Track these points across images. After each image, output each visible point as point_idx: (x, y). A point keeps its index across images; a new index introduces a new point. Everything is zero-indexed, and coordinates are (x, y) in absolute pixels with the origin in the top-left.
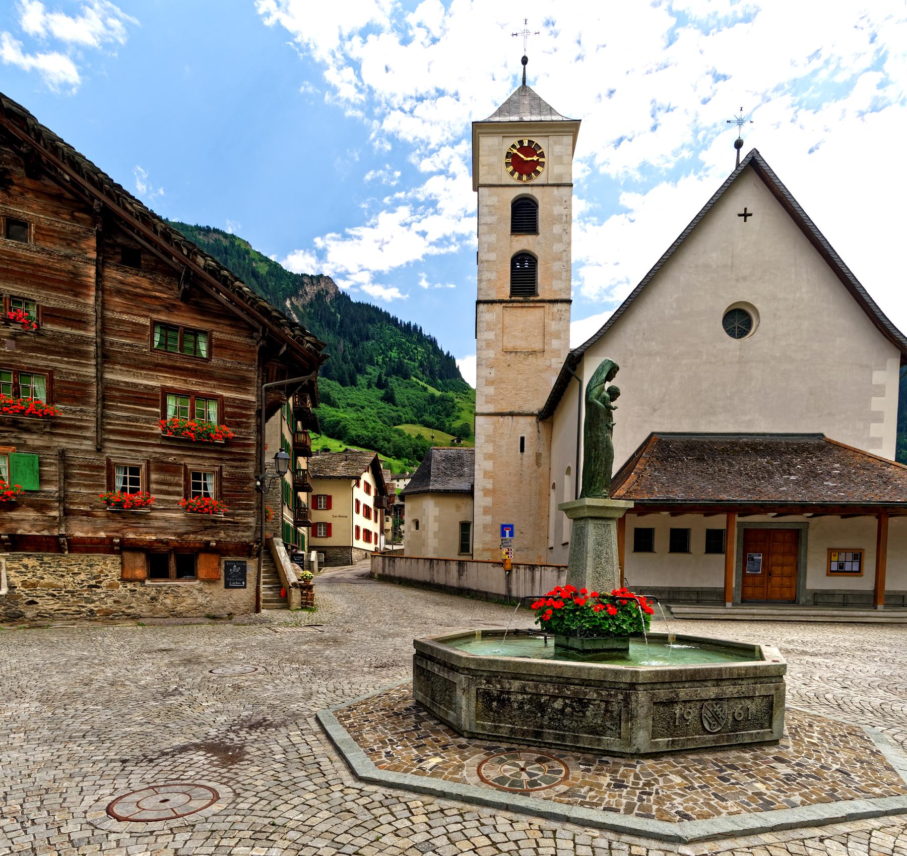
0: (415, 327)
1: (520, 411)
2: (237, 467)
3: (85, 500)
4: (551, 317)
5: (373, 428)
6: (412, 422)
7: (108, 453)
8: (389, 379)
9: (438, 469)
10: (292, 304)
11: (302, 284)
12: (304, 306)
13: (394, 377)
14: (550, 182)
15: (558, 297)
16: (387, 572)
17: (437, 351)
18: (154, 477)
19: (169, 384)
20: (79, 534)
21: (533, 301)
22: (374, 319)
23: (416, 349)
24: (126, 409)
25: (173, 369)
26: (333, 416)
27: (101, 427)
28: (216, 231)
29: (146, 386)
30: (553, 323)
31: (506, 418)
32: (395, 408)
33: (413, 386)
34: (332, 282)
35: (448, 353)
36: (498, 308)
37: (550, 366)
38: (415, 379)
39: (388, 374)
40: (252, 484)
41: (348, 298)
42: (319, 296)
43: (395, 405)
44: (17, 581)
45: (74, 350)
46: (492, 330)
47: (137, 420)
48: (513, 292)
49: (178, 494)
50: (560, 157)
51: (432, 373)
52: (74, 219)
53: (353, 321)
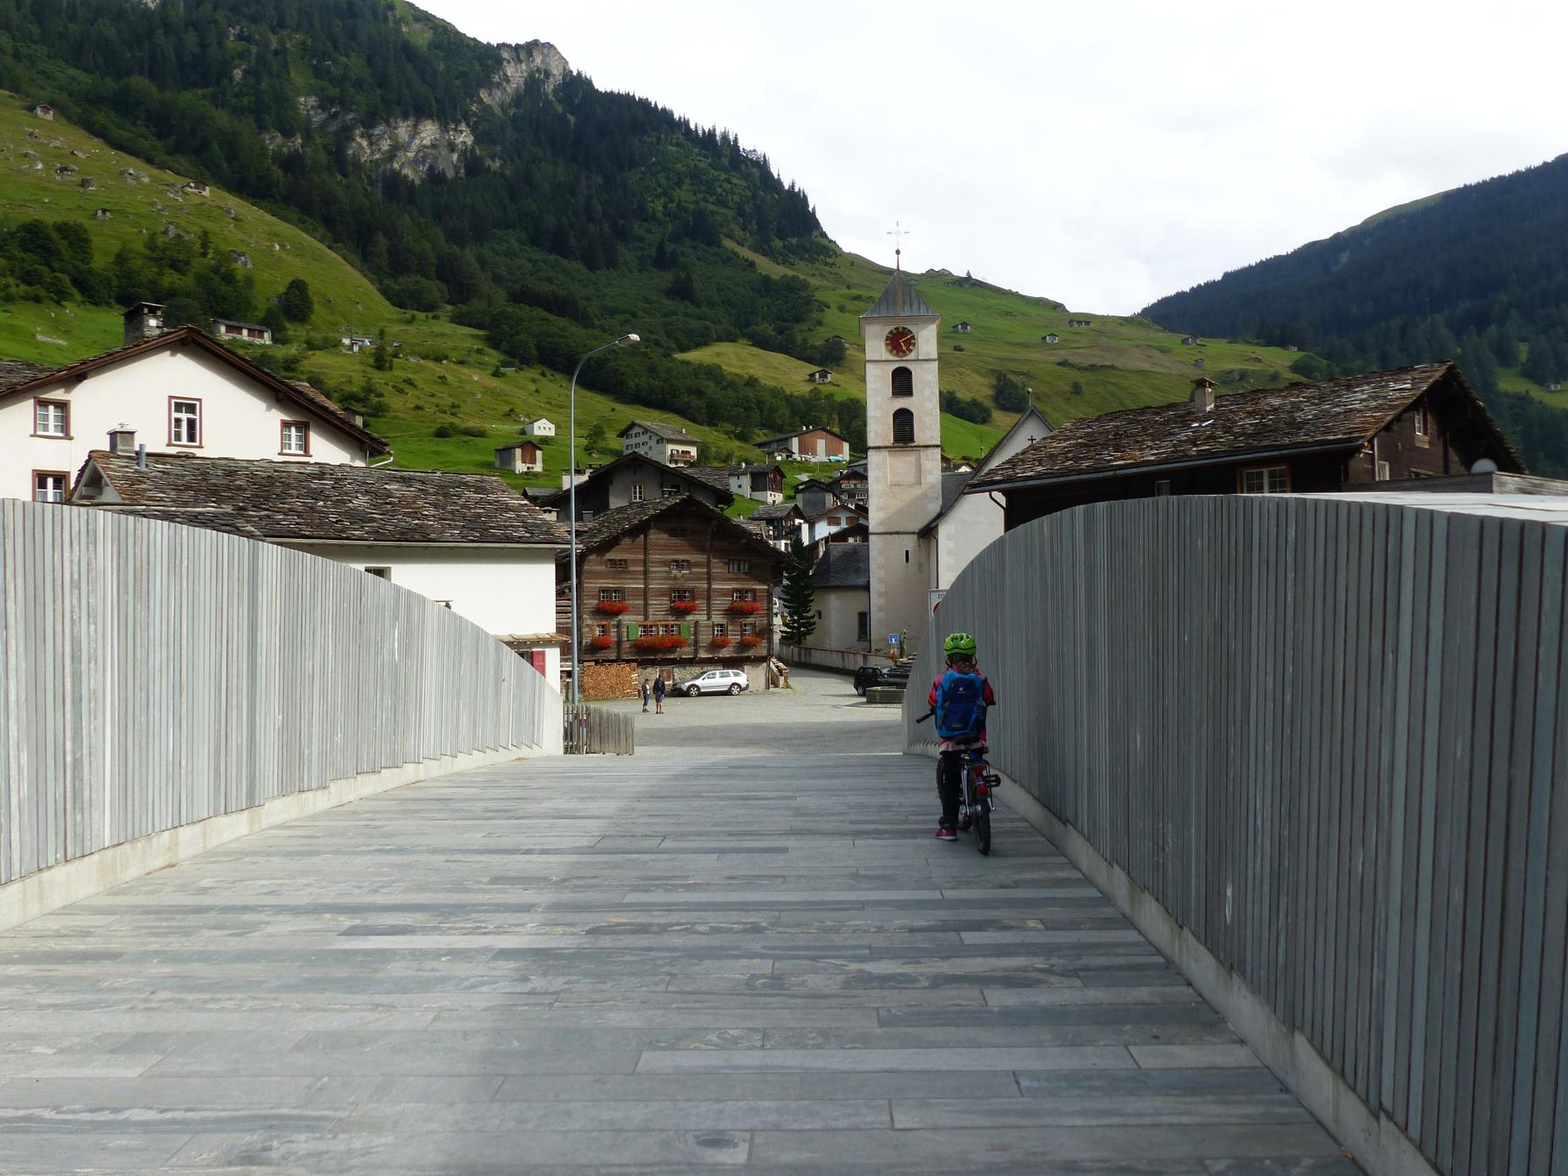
0: (725, 137)
7: (713, 619)
13: (688, 241)
16: (803, 659)
17: (772, 184)
23: (729, 181)
33: (727, 261)
36: (885, 453)
42: (533, 84)
48: (896, 439)
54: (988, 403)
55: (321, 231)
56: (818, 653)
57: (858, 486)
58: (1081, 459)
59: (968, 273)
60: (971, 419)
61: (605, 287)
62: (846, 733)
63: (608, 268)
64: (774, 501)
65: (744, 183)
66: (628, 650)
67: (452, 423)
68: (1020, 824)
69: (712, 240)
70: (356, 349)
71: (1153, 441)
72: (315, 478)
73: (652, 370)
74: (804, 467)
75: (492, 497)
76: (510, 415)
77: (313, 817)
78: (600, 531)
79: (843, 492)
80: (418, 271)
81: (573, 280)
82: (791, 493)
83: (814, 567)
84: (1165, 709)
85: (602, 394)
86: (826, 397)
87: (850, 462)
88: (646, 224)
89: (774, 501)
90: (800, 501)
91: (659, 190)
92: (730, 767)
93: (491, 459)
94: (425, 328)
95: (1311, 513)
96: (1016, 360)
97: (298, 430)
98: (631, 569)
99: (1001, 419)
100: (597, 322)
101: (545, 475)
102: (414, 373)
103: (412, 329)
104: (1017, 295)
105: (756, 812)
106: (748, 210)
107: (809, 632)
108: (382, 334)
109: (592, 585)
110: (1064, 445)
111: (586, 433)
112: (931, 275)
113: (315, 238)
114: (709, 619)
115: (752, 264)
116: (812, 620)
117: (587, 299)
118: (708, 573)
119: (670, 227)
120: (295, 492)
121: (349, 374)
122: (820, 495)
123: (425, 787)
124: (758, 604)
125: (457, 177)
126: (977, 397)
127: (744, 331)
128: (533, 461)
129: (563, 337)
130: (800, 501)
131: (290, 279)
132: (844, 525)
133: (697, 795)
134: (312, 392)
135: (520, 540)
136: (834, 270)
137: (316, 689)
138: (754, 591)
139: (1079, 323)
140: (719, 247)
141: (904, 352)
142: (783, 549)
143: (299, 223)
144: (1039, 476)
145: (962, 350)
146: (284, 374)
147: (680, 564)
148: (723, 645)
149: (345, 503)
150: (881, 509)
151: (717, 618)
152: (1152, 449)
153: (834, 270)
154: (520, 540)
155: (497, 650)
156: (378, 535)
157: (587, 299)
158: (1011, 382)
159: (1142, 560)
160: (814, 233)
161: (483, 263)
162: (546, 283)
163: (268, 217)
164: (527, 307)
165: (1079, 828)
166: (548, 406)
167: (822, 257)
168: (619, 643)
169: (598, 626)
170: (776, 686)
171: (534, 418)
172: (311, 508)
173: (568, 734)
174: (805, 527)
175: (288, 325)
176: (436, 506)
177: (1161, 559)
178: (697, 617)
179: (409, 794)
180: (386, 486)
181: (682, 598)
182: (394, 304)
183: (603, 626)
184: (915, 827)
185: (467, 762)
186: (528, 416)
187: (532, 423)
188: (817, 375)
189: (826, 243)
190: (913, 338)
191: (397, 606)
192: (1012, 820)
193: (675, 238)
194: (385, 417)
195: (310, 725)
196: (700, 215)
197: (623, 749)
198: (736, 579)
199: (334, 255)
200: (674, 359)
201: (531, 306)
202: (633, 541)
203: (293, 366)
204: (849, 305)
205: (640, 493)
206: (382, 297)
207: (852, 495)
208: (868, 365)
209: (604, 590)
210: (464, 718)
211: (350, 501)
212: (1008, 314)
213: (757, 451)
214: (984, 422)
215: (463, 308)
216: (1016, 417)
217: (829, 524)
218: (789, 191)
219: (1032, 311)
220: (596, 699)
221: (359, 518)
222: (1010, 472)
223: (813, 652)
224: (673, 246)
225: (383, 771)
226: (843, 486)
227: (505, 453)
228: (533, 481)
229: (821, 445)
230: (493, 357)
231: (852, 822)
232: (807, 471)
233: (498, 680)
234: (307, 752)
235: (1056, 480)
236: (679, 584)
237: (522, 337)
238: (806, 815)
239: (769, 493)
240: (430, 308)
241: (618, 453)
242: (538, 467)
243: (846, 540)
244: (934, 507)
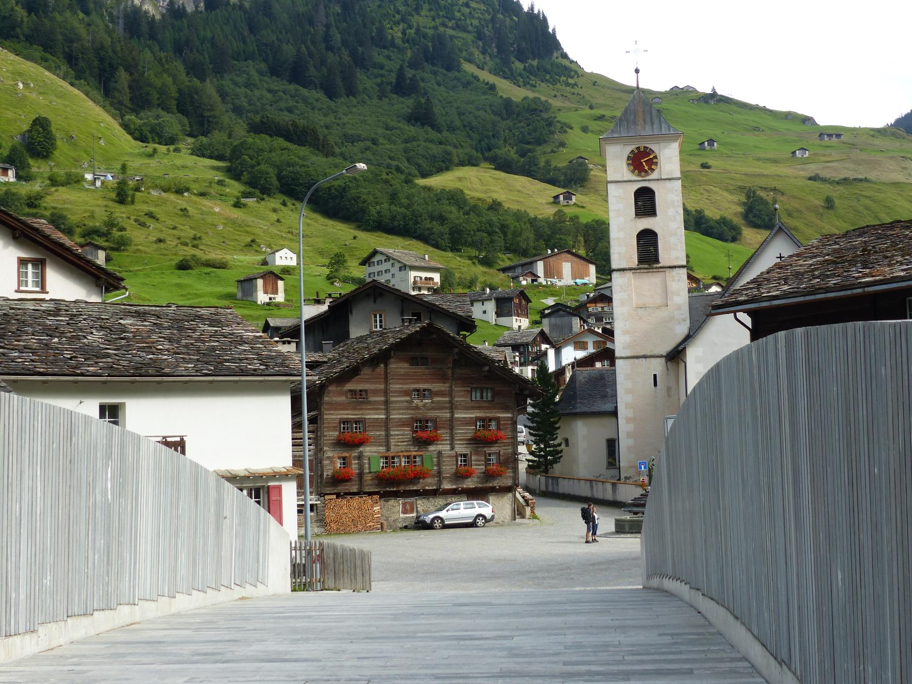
1: (652, 354)
2: (506, 449)
8: (419, 74)
13: (428, 67)
16: (550, 489)
21: (656, 268)
24: (462, 429)
30: (674, 283)
36: (629, 274)
43: (436, 128)
48: (641, 261)
51: (501, 50)
54: (738, 221)
55: (64, 68)
56: (566, 482)
57: (606, 309)
58: (828, 276)
59: (714, 89)
60: (721, 238)
61: (346, 115)
62: (593, 565)
63: (348, 96)
64: (520, 327)
65: (483, 7)
66: (370, 482)
67: (194, 256)
68: (741, 664)
69: (451, 65)
70: (98, 183)
71: (903, 256)
72: (50, 315)
73: (393, 197)
74: (550, 291)
75: (227, 330)
76: (252, 245)
77: (19, 663)
78: (339, 362)
79: (589, 315)
80: (159, 105)
81: (313, 109)
82: (537, 318)
83: (561, 393)
84: (861, 543)
85: (343, 223)
86: (571, 219)
87: (597, 285)
88: (386, 52)
89: (520, 327)
90: (546, 326)
91: (398, 17)
92: (455, 605)
93: (233, 289)
94: (166, 161)
95: (295, 442)
96: (767, 176)
97: (35, 266)
98: (372, 399)
99: (752, 236)
100: (337, 150)
101: (288, 306)
102: (156, 206)
103: (152, 162)
104: (764, 110)
105: (467, 653)
106: (487, 33)
107: (556, 461)
108: (124, 168)
109: (332, 416)
110: (810, 262)
111: (327, 261)
112: (677, 94)
113: (58, 76)
114: (452, 448)
115: (492, 88)
116: (559, 448)
117: (327, 127)
118: (451, 402)
119: (409, 53)
120: (30, 330)
121: (92, 208)
122: (566, 319)
123: (138, 630)
124: (502, 433)
125: (197, 11)
126: (726, 215)
127: (486, 154)
128: (275, 292)
129: (303, 166)
130: (546, 326)
131: (34, 117)
132: (591, 350)
133: (411, 636)
134: (49, 230)
135: (255, 373)
136: (576, 90)
137: (24, 531)
138: (498, 420)
139: (830, 136)
140: (459, 71)
141: (646, 171)
142: (530, 375)
143: (43, 62)
144: (785, 296)
145: (708, 167)
146: (27, 210)
147: (421, 394)
148: (466, 476)
149: (79, 339)
150: (627, 332)
151: (460, 449)
152: (902, 264)
153: (576, 90)
154: (255, 373)
155: (218, 488)
156: (112, 371)
157: (327, 127)
158: (761, 198)
159: (835, 389)
160: (555, 55)
161: (223, 95)
162: (286, 113)
163: (12, 56)
164: (267, 137)
165: (793, 668)
166: (290, 235)
167: (563, 78)
168: (361, 475)
169: (339, 458)
170: (523, 517)
171: (276, 248)
172: (46, 345)
173: (297, 570)
174: (551, 353)
175: (31, 162)
176: (170, 340)
177: (851, 387)
178: (440, 447)
179: (121, 637)
180: (122, 321)
181: (424, 428)
182: (136, 139)
183: (344, 458)
184: (629, 668)
185: (183, 603)
186: (269, 246)
187: (274, 253)
188: (561, 197)
189: (565, 62)
190: (656, 157)
191: (110, 446)
192: (732, 660)
193: (413, 65)
194: (127, 250)
195: (18, 568)
196: (440, 41)
197: (360, 585)
198: (479, 408)
199: (76, 91)
200: (416, 185)
201: (271, 136)
202: (373, 371)
203: (36, 203)
204: (593, 125)
205: (381, 321)
206: (124, 132)
207: (599, 319)
208: (610, 186)
209: (345, 422)
210: (183, 557)
211: (85, 337)
212: (756, 129)
213: (502, 275)
214: (734, 240)
215: (204, 139)
216: (765, 233)
217: (576, 349)
218: (528, 13)
219: (781, 125)
220: (338, 533)
221: (94, 354)
222: (755, 292)
223: (560, 481)
224: (413, 72)
225: (96, 613)
226: (590, 310)
227: (247, 284)
228: (276, 312)
229: (567, 268)
230: (235, 188)
231: (565, 664)
232: (553, 295)
233: (220, 517)
234: (13, 595)
235: (802, 299)
236: (419, 414)
237: (263, 167)
238: (517, 656)
239: (514, 318)
240: (171, 141)
241: (360, 281)
242: (280, 298)
243: (593, 365)
244: (682, 329)
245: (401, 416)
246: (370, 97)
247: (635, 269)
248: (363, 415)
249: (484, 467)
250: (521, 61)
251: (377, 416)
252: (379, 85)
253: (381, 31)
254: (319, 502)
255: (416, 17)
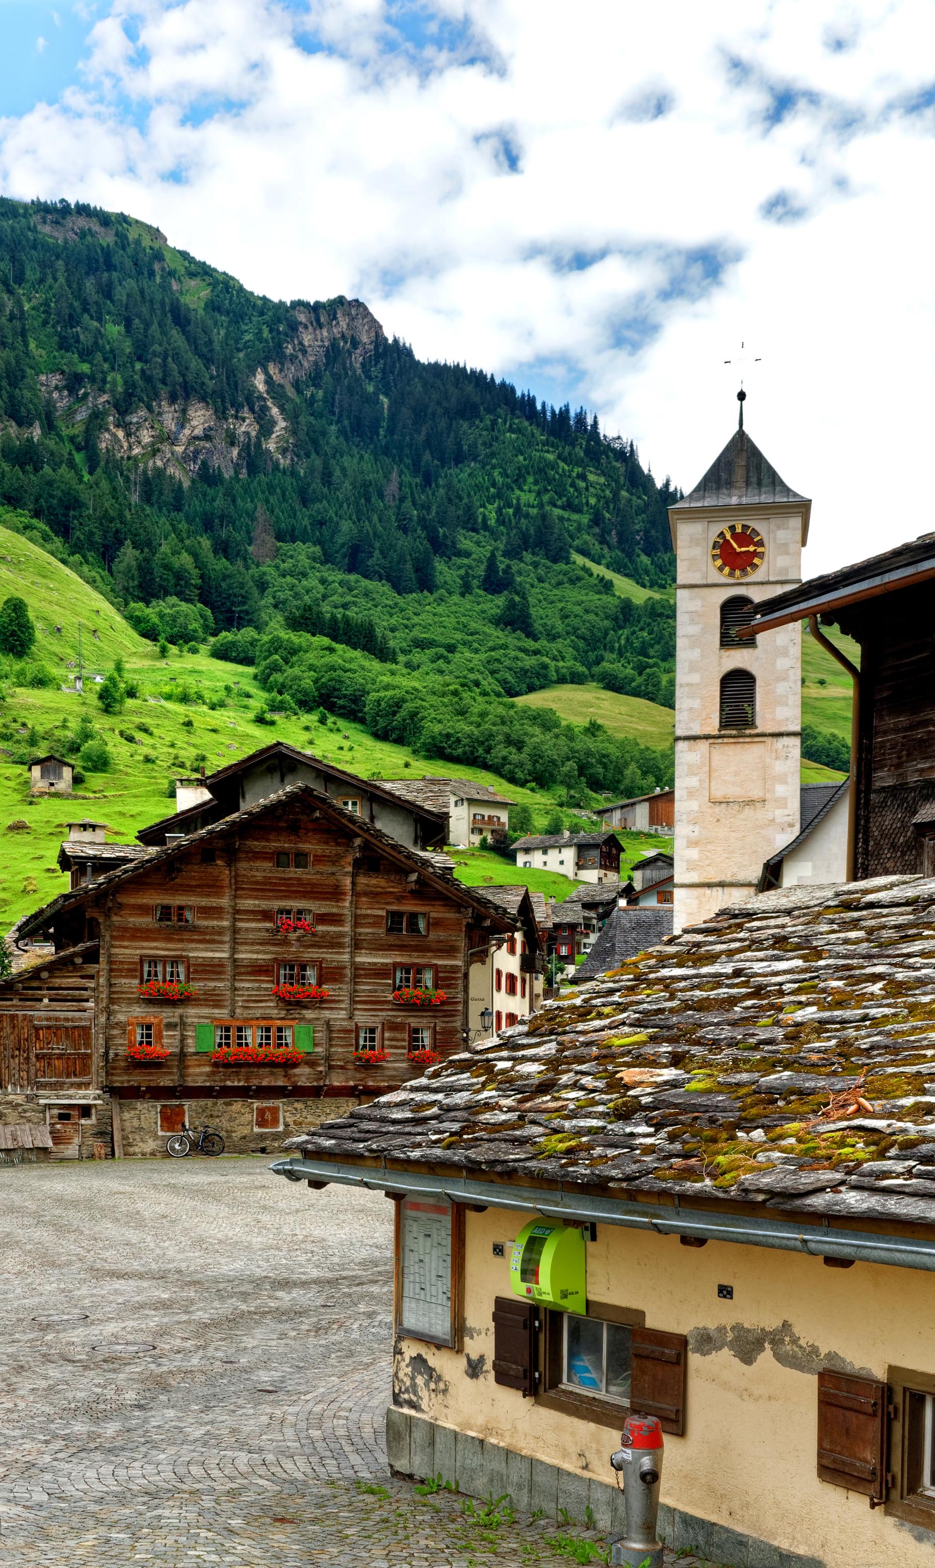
3: (341, 1056)
4: (774, 755)
5: (483, 715)
6: (576, 679)
8: (516, 566)
9: (626, 942)
10: (269, 381)
11: (294, 327)
12: (297, 385)
14: (772, 579)
15: (783, 729)
18: (387, 1035)
19: (398, 960)
20: (336, 1084)
21: (750, 736)
22: (475, 407)
23: (583, 477)
24: (368, 983)
25: (402, 948)
26: (387, 687)
27: (353, 1002)
28: (83, 210)
29: (382, 964)
30: (778, 762)
31: (715, 889)
32: (530, 644)
34: (367, 313)
35: (667, 485)
36: (703, 745)
37: (773, 820)
38: (580, 560)
39: (512, 553)
40: (459, 1036)
41: (409, 353)
42: (333, 353)
43: (531, 635)
44: (290, 1120)
45: (334, 943)
46: (696, 774)
47: (376, 991)
48: (724, 725)
49: (404, 1047)
50: (786, 545)
51: (625, 542)
52: (338, 844)
53: (420, 414)
65: (602, 480)
199: (67, 570)
224: (507, 561)
245: (255, 956)
246: (450, 593)
247: (714, 737)
248: (184, 950)
249: (405, 1051)
250: (648, 555)
251: (210, 954)
252: (462, 578)
253: (469, 509)
254: (100, 1102)
255: (518, 492)
